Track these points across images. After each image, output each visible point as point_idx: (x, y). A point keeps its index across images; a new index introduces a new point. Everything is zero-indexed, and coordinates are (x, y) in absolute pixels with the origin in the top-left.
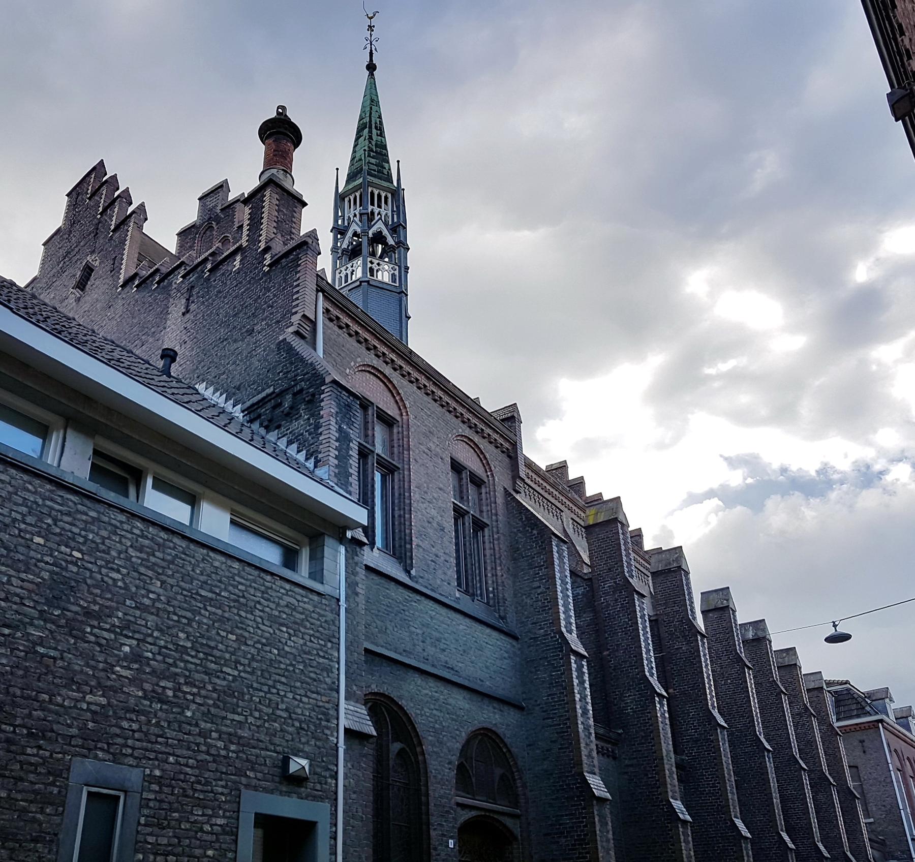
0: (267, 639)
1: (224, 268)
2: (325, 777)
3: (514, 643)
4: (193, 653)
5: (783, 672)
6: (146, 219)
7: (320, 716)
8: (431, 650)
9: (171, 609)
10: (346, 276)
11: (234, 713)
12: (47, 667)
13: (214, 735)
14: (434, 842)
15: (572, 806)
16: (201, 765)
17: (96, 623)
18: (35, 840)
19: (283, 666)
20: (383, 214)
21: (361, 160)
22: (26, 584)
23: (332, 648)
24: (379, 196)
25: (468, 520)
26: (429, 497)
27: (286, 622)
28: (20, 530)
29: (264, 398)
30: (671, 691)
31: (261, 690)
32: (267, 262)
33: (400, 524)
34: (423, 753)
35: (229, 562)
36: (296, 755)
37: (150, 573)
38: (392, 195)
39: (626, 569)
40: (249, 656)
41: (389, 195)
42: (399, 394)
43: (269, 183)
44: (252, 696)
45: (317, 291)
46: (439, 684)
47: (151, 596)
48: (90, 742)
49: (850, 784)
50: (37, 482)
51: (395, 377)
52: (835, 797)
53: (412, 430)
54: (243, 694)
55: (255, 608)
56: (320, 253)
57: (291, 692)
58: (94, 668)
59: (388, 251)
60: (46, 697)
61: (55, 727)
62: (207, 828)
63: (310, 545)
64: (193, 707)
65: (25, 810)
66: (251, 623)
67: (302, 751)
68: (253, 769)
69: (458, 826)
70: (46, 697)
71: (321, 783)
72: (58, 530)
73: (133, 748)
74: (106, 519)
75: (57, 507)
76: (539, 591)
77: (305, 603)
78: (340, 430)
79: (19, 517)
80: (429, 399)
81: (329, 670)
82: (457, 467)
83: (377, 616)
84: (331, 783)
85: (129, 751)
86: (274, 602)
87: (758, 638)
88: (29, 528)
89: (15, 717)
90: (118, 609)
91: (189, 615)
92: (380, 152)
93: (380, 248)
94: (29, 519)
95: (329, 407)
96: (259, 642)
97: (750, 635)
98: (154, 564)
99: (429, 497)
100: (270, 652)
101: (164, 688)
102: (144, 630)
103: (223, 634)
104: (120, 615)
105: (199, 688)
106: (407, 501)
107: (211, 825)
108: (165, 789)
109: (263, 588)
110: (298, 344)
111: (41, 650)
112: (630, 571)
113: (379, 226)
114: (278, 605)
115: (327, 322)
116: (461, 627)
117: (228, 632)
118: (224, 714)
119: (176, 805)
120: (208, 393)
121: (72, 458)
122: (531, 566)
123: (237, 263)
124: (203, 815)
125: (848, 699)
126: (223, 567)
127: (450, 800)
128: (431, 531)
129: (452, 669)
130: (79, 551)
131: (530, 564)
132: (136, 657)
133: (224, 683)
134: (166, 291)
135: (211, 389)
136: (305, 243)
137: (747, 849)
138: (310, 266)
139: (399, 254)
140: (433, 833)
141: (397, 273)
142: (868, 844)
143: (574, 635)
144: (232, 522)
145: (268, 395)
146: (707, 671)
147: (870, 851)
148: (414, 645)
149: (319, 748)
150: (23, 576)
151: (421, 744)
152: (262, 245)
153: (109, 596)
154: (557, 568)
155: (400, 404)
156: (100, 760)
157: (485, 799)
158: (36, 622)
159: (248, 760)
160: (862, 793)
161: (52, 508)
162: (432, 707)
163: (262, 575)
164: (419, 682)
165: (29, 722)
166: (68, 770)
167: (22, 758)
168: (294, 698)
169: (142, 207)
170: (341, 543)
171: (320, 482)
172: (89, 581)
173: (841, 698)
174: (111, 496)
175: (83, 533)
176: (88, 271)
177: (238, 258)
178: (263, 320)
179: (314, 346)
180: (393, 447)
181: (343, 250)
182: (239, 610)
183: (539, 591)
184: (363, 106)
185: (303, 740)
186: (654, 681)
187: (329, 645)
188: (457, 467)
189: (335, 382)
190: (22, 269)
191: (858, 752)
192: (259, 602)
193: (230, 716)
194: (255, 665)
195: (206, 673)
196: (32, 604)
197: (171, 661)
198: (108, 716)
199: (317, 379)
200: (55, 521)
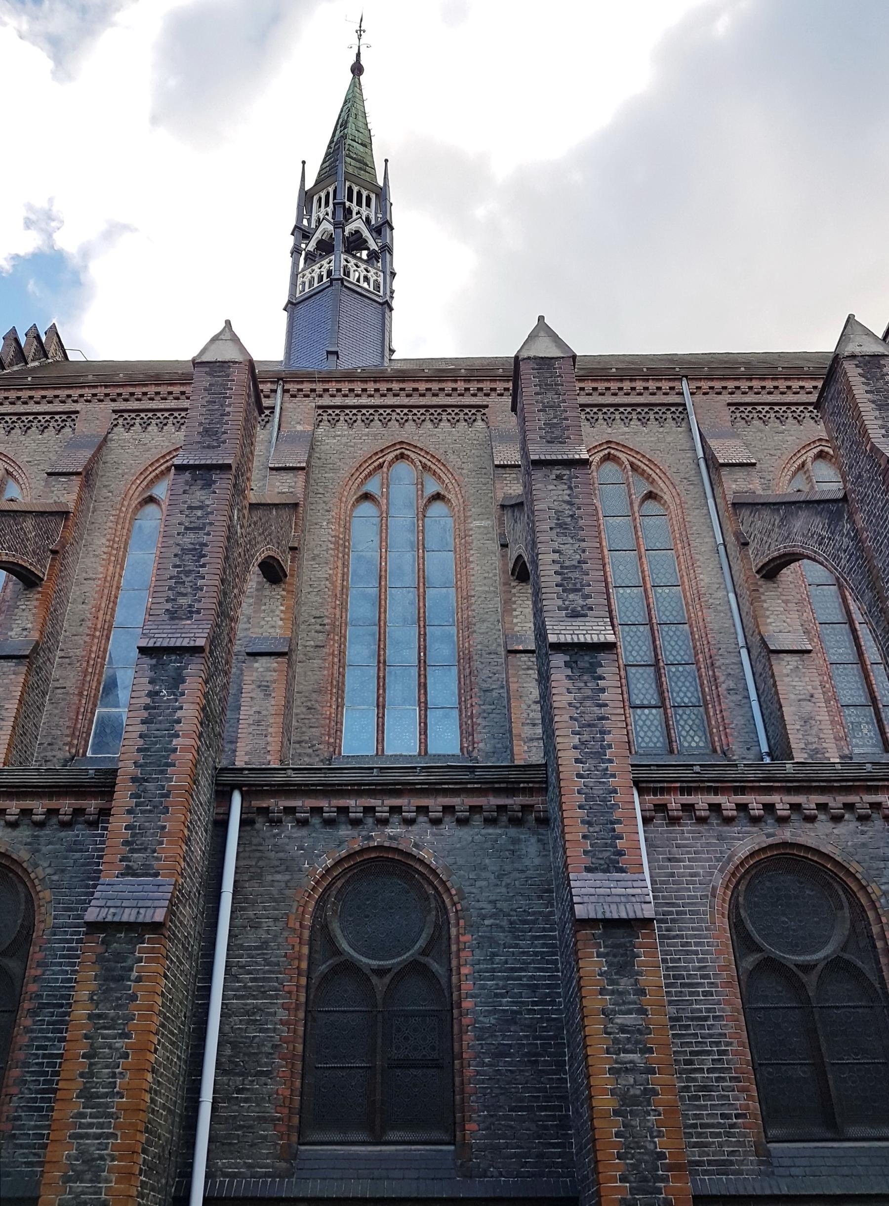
24: (359, 195)
38: (377, 195)
41: (373, 196)
157: (361, 1137)
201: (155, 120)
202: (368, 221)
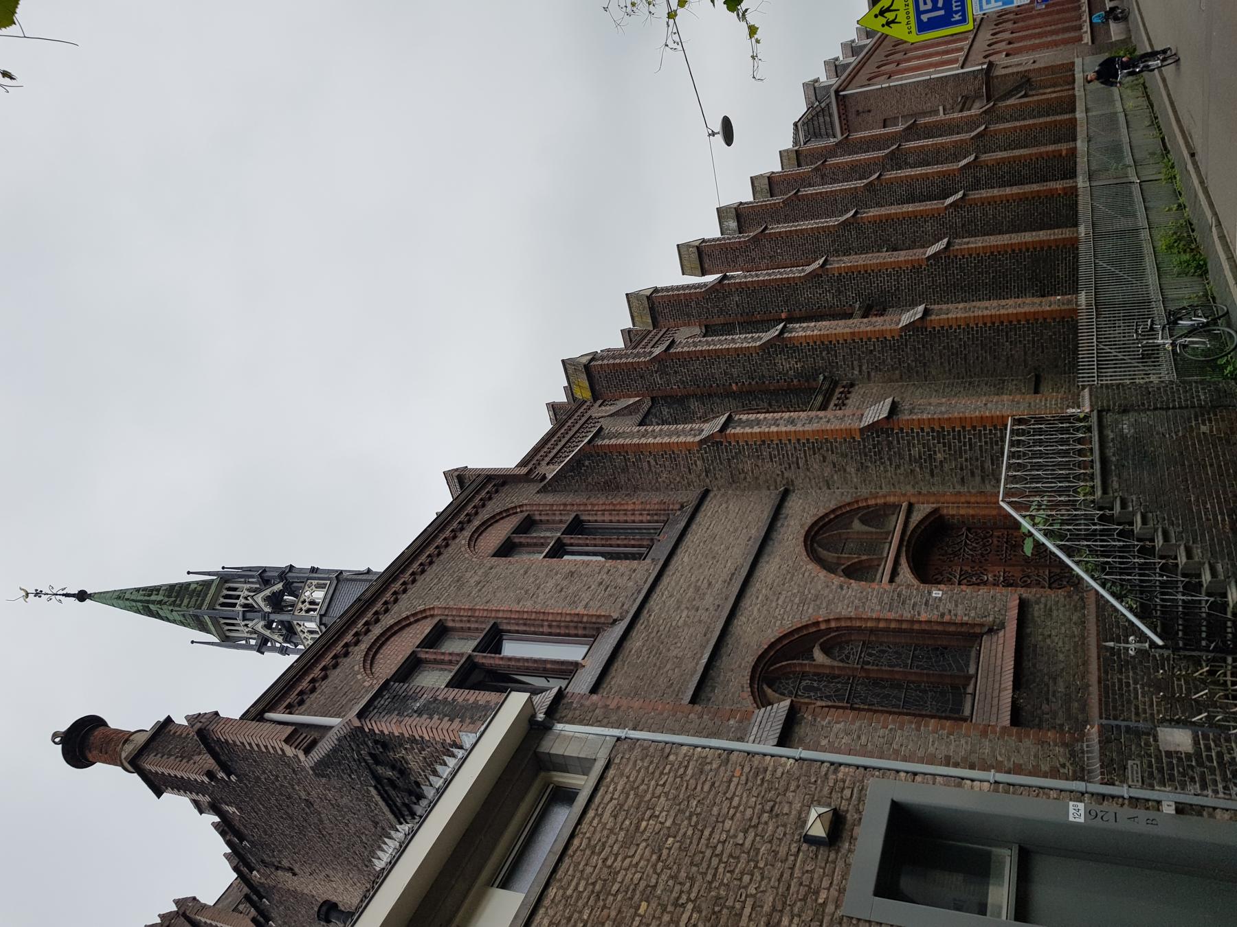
0: (653, 852)
1: (237, 823)
2: (836, 781)
3: (711, 495)
5: (776, 191)
6: (194, 899)
7: (759, 782)
8: (709, 600)
11: (740, 915)
14: (934, 616)
15: (898, 443)
19: (690, 832)
20: (247, 593)
21: (184, 616)
23: (677, 755)
24: (226, 597)
26: (532, 589)
27: (635, 822)
29: (383, 798)
31: (717, 869)
33: (559, 627)
34: (828, 621)
35: (547, 902)
36: (805, 822)
38: (226, 582)
39: (642, 359)
40: (671, 883)
41: (227, 585)
42: (407, 618)
43: (135, 765)
44: (722, 883)
46: (748, 595)
49: (900, 127)
51: (388, 621)
53: (451, 604)
54: (718, 898)
55: (610, 867)
56: (216, 713)
57: (723, 822)
59: (290, 588)
63: (549, 770)
66: (630, 875)
67: (800, 813)
68: (817, 893)
69: (915, 582)
71: (843, 789)
76: (653, 462)
77: (615, 789)
78: (419, 712)
80: (420, 579)
81: (703, 761)
82: (506, 550)
83: (659, 668)
84: (846, 774)
86: (608, 837)
87: (737, 215)
95: (386, 725)
96: (654, 866)
97: (733, 224)
99: (532, 589)
100: (670, 849)
106: (533, 616)
109: (588, 852)
110: (324, 747)
112: (645, 354)
114: (611, 831)
115: (304, 707)
116: (686, 559)
122: (625, 470)
123: (231, 809)
126: (551, 912)
127: (885, 591)
128: (572, 589)
129: (733, 574)
135: (380, 853)
136: (200, 733)
137: (960, 244)
140: (924, 617)
142: (965, 113)
144: (505, 885)
145: (380, 794)
147: (973, 112)
148: (700, 621)
149: (798, 786)
151: (817, 623)
152: (206, 780)
154: (628, 441)
155: (419, 617)
157: (887, 546)
159: (804, 900)
162: (774, 604)
163: (570, 852)
164: (743, 619)
168: (732, 819)
170: (550, 728)
173: (811, 130)
179: (328, 728)
180: (469, 628)
182: (609, 893)
183: (653, 462)
185: (786, 810)
186: (766, 336)
187: (672, 758)
188: (506, 550)
189: (361, 715)
192: (605, 860)
194: (683, 874)
199: (355, 736)
202: (257, 591)
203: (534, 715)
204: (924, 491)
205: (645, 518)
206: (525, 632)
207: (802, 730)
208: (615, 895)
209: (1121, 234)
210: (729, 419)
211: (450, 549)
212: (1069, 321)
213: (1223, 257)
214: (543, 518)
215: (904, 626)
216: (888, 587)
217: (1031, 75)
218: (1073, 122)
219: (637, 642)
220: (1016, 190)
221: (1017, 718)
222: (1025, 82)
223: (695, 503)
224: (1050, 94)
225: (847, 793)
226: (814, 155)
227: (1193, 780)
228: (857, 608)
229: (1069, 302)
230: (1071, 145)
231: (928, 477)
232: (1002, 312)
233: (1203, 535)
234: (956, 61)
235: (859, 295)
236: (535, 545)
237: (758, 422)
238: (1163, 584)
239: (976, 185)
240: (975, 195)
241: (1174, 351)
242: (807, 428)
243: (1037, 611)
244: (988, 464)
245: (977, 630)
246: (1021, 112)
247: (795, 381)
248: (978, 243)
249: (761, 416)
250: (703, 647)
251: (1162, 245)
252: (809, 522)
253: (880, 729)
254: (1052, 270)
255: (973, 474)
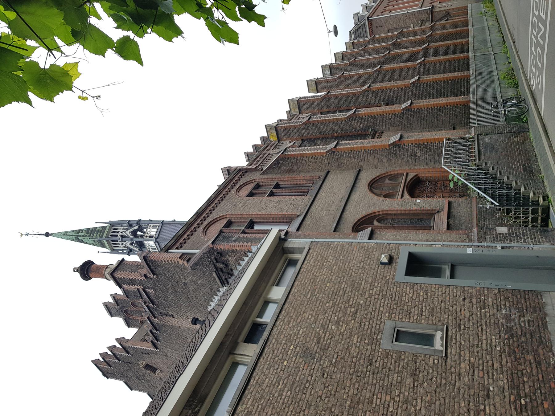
1: (152, 297)
3: (330, 173)
4: (335, 300)
5: (345, 59)
9: (316, 309)
10: (152, 249)
12: (341, 359)
13: (371, 292)
14: (418, 208)
16: (384, 297)
17: (322, 340)
18: (416, 363)
20: (122, 230)
21: (94, 241)
22: (305, 368)
25: (275, 191)
28: (281, 370)
30: (353, 108)
32: (152, 276)
33: (276, 219)
35: (295, 286)
37: (300, 318)
41: (113, 227)
45: (167, 252)
47: (310, 317)
48: (374, 341)
49: (396, 33)
50: (259, 364)
51: (209, 220)
52: (402, 40)
53: (233, 213)
58: (342, 340)
59: (141, 229)
60: (354, 359)
61: (367, 355)
62: (411, 295)
63: (287, 253)
64: (358, 300)
65: (403, 367)
68: (386, 277)
70: (354, 359)
72: (281, 355)
73: (377, 324)
74: (276, 336)
75: (271, 356)
76: (307, 161)
78: (235, 241)
79: (275, 371)
80: (219, 206)
81: (343, 246)
82: (251, 195)
85: (378, 326)
88: (280, 367)
89: (363, 371)
90: (316, 331)
91: (318, 302)
92: (91, 232)
93: (139, 233)
94: (276, 367)
95: (222, 246)
96: (330, 274)
97: (328, 73)
98: (296, 316)
99: (265, 207)
101: (350, 312)
102: (325, 320)
103: (327, 288)
104: (318, 330)
105: (350, 298)
107: (410, 293)
108: (394, 312)
110: (193, 261)
111: (334, 361)
112: (299, 122)
113: (128, 233)
114: (314, 266)
115: (183, 248)
116: (323, 194)
117: (326, 286)
118: (362, 288)
119: (401, 307)
120: (213, 304)
121: (249, 351)
124: (405, 296)
125: (356, 32)
130: (290, 346)
131: (295, 165)
132: (337, 323)
133: (348, 288)
134: (161, 326)
136: (144, 257)
138: (155, 255)
139: (143, 223)
141: (152, 225)
143: (327, 146)
144: (277, 285)
146: (344, 91)
150: (301, 369)
151: (375, 213)
153: (310, 334)
154: (298, 153)
156: (382, 337)
158: (322, 363)
159: (382, 279)
160: (400, 28)
161: (271, 358)
165: (365, 365)
166: (386, 350)
167: (381, 368)
169: (118, 340)
171: (258, 250)
172: (304, 342)
174: (266, 334)
175: (282, 345)
176: (148, 367)
177: (148, 290)
178: (180, 278)
181: (140, 250)
183: (307, 161)
184: (67, 239)
185: (373, 256)
188: (251, 195)
189: (213, 243)
190: (143, 400)
191: (382, 29)
192: (313, 274)
193: (363, 285)
194: (340, 276)
195: (344, 295)
196: (314, 365)
197: (339, 309)
198: (363, 334)
199: (210, 251)
200: (276, 356)
201: (52, 101)
203: (280, 236)
204: (412, 168)
205: (304, 182)
206: (263, 222)
207: (375, 236)
208: (318, 282)
209: (487, 73)
210: (337, 143)
211: (229, 195)
212: (466, 106)
213: (523, 79)
214: (264, 184)
215: (407, 212)
216: (401, 200)
217: (450, 11)
218: (468, 30)
219: (308, 221)
220: (445, 57)
221: (449, 228)
222: (447, 14)
223: (324, 176)
224: (458, 19)
225: (394, 251)
226: (360, 45)
227: (507, 240)
228: (389, 207)
229: (466, 98)
230: (467, 39)
231: (414, 162)
232: (441, 102)
233: (513, 172)
234: (418, 5)
235: (383, 99)
236: (262, 193)
237: (349, 144)
238: (499, 188)
239: (429, 55)
240: (428, 59)
241: (505, 113)
242: (368, 145)
243: (455, 205)
244: (436, 157)
245: (434, 212)
246: (446, 27)
247: (360, 132)
248: (430, 77)
249: (350, 142)
250: (333, 222)
251: (501, 77)
252: (370, 180)
253: (404, 233)
254: (460, 87)
255: (431, 161)
